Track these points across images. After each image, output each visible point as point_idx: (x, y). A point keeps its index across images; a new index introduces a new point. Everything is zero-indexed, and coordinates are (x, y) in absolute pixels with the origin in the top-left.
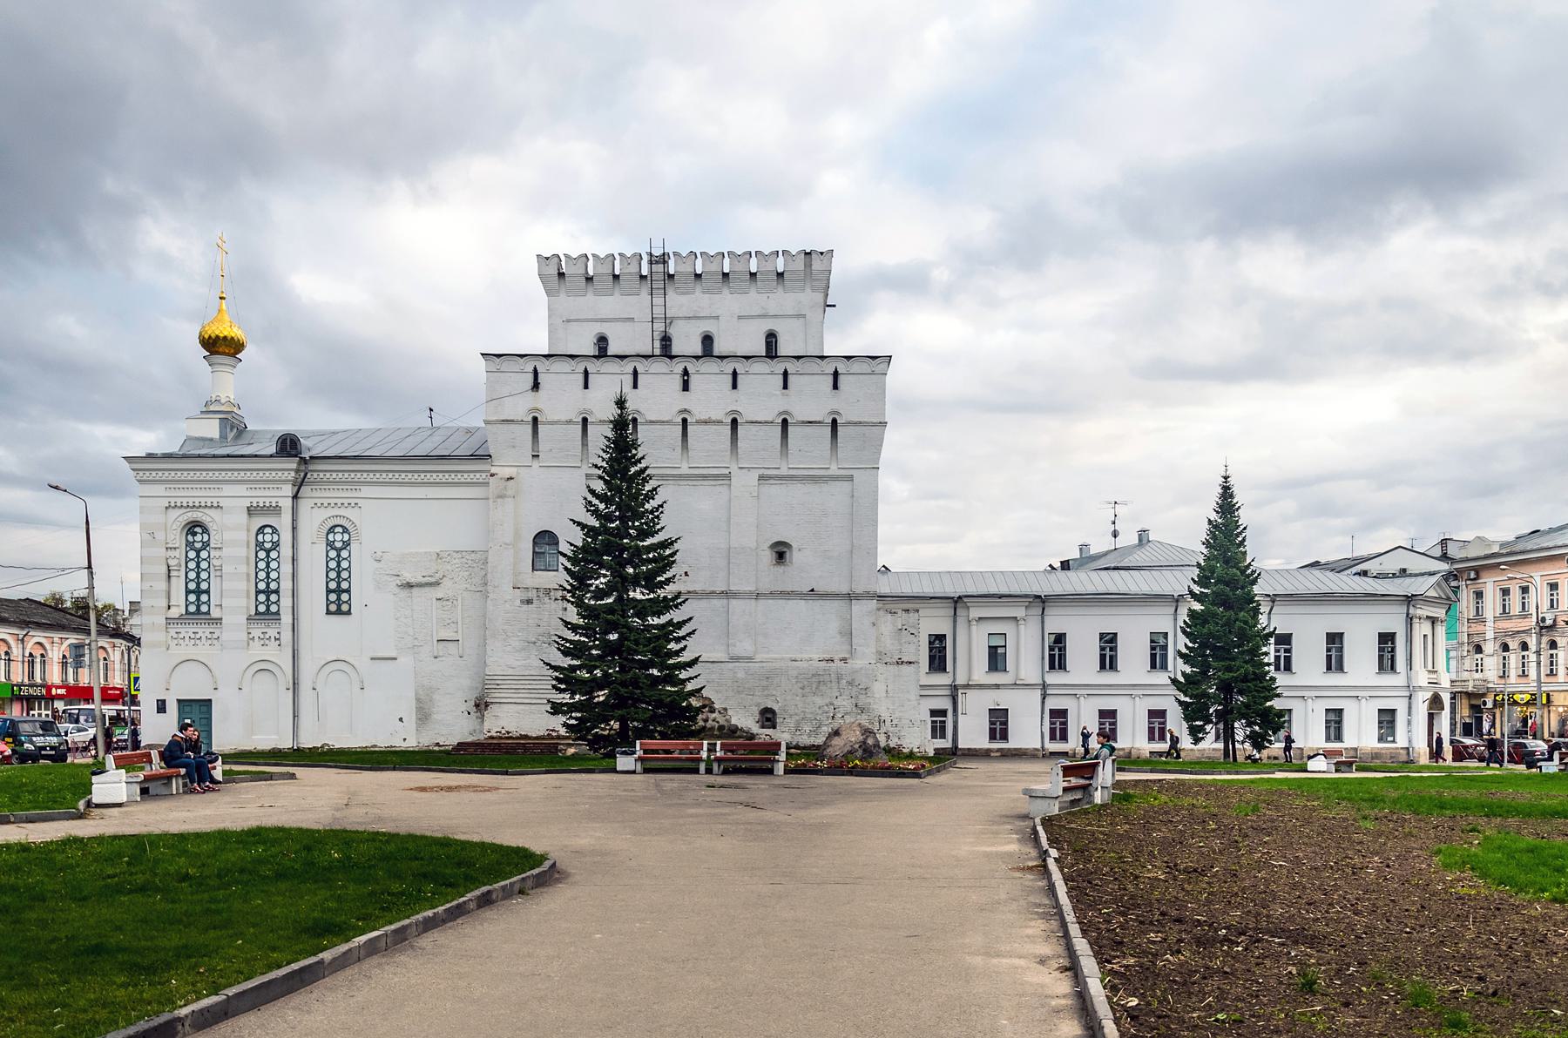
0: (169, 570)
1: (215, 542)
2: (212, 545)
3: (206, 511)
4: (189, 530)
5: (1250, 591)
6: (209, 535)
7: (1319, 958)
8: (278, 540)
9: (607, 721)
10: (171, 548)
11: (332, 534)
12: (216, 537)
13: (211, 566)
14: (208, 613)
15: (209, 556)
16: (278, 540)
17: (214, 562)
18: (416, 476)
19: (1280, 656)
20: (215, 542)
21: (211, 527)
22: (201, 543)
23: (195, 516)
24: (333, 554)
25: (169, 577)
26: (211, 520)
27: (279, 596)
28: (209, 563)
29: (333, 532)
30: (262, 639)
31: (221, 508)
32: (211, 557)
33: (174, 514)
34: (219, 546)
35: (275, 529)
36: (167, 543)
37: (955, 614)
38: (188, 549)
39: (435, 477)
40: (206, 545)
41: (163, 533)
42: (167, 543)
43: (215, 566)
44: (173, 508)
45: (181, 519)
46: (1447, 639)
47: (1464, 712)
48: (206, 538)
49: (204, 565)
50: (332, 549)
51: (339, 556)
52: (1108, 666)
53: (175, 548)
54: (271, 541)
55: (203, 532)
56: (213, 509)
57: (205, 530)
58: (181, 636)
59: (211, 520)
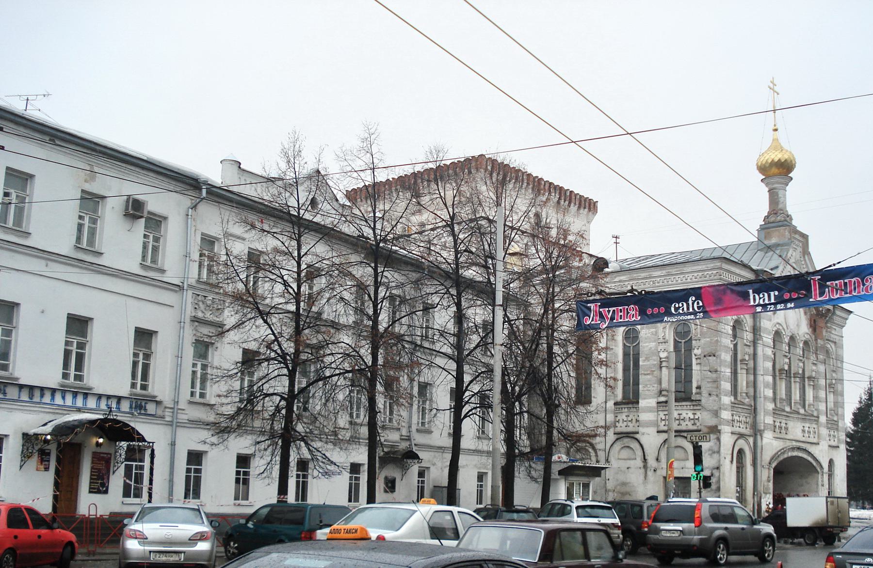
0: (661, 362)
43: (695, 355)
58: (630, 419)
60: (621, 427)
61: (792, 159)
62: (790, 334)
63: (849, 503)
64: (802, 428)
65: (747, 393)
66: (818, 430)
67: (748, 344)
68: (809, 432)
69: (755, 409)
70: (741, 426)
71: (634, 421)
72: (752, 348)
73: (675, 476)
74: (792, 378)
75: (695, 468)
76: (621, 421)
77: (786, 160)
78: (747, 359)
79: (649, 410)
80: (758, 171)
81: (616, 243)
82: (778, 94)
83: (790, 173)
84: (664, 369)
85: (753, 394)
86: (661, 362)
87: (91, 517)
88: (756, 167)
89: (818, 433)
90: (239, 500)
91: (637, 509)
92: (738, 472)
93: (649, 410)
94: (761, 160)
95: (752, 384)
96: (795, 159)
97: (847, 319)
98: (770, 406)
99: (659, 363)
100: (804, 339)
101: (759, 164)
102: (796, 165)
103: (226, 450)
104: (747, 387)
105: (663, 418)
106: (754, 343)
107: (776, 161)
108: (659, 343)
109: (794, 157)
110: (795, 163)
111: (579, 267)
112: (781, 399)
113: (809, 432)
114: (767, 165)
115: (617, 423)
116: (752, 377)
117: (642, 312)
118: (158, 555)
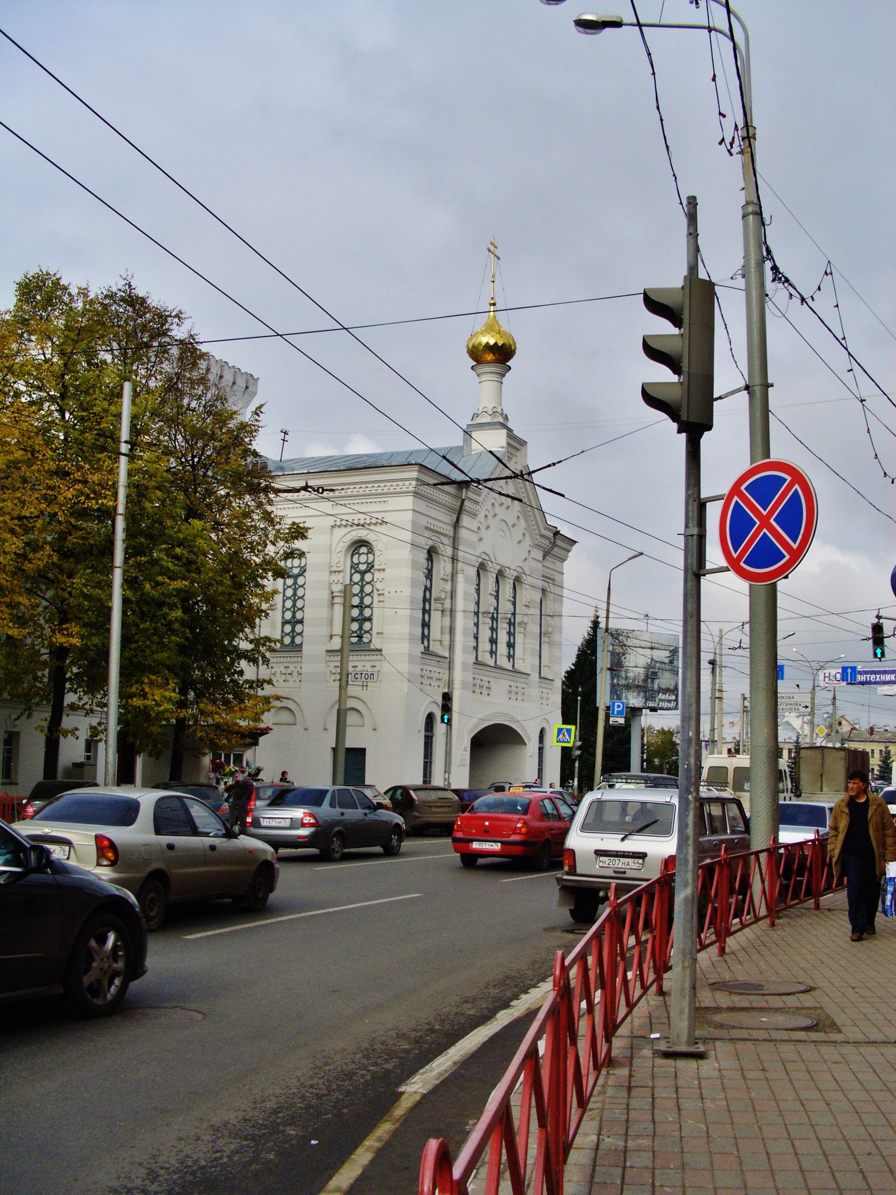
4: (354, 551)
6: (374, 555)
7: (322, 1099)
8: (373, 561)
9: (248, 693)
10: (335, 572)
12: (380, 558)
13: (375, 591)
16: (373, 561)
17: (378, 585)
22: (366, 565)
24: (357, 577)
27: (372, 624)
28: (373, 586)
29: (358, 553)
32: (375, 580)
33: (339, 533)
36: (331, 566)
37: (650, 1019)
38: (353, 571)
40: (370, 567)
41: (328, 555)
42: (331, 566)
43: (378, 590)
44: (339, 526)
45: (345, 539)
46: (4, 745)
47: (56, 436)
49: (368, 589)
50: (357, 572)
51: (362, 579)
53: (339, 572)
54: (366, 562)
55: (369, 553)
57: (371, 551)
58: (289, 671)
61: (512, 343)
63: (7, 794)
65: (441, 641)
67: (446, 577)
71: (295, 674)
72: (449, 583)
73: (347, 746)
74: (123, 460)
76: (278, 674)
80: (468, 355)
81: (284, 440)
82: (499, 259)
83: (508, 361)
86: (333, 598)
88: (466, 349)
90: (737, 769)
91: (724, 770)
94: (473, 341)
95: (448, 630)
96: (515, 344)
97: (569, 551)
101: (470, 345)
102: (517, 351)
103: (77, 733)
105: (334, 671)
108: (331, 572)
109: (514, 341)
110: (516, 348)
114: (481, 348)
116: (447, 620)
117: (104, 432)
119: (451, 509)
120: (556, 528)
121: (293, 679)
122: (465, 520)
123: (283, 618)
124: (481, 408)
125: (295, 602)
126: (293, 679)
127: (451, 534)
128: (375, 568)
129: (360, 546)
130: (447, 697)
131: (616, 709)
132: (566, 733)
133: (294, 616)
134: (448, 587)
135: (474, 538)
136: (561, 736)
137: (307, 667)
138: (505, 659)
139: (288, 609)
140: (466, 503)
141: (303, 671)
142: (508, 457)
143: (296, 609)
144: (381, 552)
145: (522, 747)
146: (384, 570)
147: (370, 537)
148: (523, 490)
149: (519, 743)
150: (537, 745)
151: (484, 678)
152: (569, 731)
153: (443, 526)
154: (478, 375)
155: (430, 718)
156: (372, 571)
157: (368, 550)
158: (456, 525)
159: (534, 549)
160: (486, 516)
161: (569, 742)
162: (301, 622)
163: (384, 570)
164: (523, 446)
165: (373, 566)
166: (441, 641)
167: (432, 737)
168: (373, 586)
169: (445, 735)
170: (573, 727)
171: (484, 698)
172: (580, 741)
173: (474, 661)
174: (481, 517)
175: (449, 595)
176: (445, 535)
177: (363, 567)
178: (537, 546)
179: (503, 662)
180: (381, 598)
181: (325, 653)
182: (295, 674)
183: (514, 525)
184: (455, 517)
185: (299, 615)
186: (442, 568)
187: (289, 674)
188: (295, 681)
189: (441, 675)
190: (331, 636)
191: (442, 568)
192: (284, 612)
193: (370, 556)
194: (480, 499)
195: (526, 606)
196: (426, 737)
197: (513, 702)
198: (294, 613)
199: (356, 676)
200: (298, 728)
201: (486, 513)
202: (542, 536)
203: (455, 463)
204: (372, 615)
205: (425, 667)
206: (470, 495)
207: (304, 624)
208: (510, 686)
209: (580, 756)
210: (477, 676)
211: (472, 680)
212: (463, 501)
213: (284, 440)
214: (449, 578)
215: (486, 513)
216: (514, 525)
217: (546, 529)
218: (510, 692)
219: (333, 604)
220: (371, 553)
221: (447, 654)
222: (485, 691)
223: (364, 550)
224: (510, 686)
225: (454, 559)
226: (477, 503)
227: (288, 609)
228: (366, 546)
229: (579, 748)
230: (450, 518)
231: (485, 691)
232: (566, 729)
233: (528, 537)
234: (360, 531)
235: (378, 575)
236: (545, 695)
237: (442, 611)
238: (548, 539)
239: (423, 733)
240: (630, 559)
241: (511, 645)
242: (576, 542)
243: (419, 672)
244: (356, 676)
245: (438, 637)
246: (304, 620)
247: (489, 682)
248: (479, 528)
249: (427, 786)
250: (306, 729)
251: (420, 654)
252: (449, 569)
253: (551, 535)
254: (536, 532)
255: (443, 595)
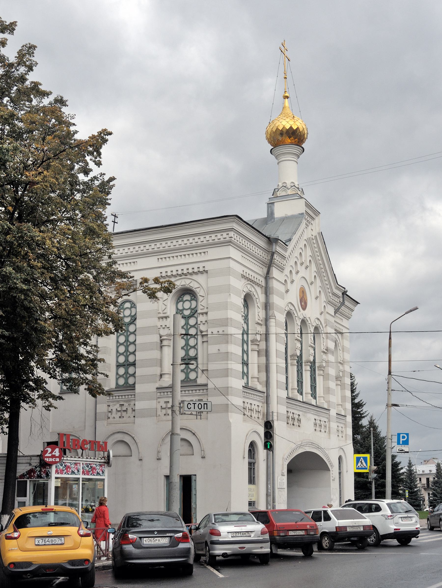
0: (161, 341)
1: (202, 308)
2: (199, 311)
3: (194, 277)
5: (81, 359)
8: (136, 314)
11: (181, 303)
13: (199, 333)
14: (195, 380)
15: (197, 323)
18: (131, 249)
19: (251, 468)
20: (202, 308)
21: (200, 292)
23: (183, 283)
25: (161, 347)
26: (198, 286)
30: (119, 411)
31: (207, 272)
32: (199, 323)
34: (205, 311)
35: (133, 303)
39: (142, 248)
40: (194, 312)
43: (201, 332)
48: (194, 303)
52: (389, 489)
56: (200, 275)
58: (124, 408)
59: (198, 286)
60: (114, 418)
62: (302, 317)
64: (314, 421)
65: (258, 378)
66: (329, 424)
67: (260, 322)
68: (320, 426)
69: (268, 397)
70: (257, 408)
71: (130, 411)
72: (264, 327)
75: (197, 377)
76: (114, 410)
77: (298, 128)
78: (259, 339)
79: (147, 396)
81: (114, 222)
84: (165, 349)
85: (265, 379)
87: (429, 528)
89: (329, 427)
92: (250, 469)
93: (147, 396)
98: (283, 394)
99: (159, 342)
100: (315, 324)
104: (259, 371)
106: (267, 320)
107: (288, 128)
111: (88, 273)
112: (292, 389)
113: (320, 426)
115: (110, 414)
116: (263, 360)
118: (237, 534)
119: (263, 263)
120: (344, 288)
121: (128, 415)
122: (275, 272)
123: (117, 361)
124: (281, 185)
125: (127, 347)
126: (128, 415)
127: (263, 284)
128: (198, 312)
129: (184, 294)
130: (268, 425)
131: (401, 440)
132: (363, 461)
133: (127, 360)
134: (262, 330)
135: (282, 288)
136: (359, 464)
137: (140, 405)
138: (310, 397)
139: (121, 344)
140: (275, 256)
141: (137, 408)
142: (306, 224)
143: (128, 353)
144: (203, 298)
145: (329, 472)
146: (206, 313)
147: (194, 285)
148: (318, 254)
149: (327, 470)
150: (338, 471)
151: (295, 412)
152: (365, 459)
153: (256, 276)
154: (276, 158)
155: (252, 445)
156: (196, 315)
157: (191, 297)
158: (267, 276)
159: (328, 305)
160: (291, 271)
161: (366, 469)
162: (134, 364)
163: (206, 313)
164: (317, 216)
165: (197, 311)
166: (258, 378)
167: (254, 463)
168: (197, 329)
169: (266, 461)
170: (368, 456)
171: (296, 429)
172: (375, 465)
173: (287, 396)
174: (287, 271)
175: (264, 336)
176: (258, 285)
177: (187, 313)
178: (330, 302)
179: (308, 398)
180: (205, 339)
181: (155, 390)
182: (130, 411)
183: (312, 283)
184: (265, 270)
185: (131, 359)
186: (257, 314)
187: (124, 411)
188: (129, 417)
189: (260, 408)
190: (161, 376)
191: (257, 314)
192: (117, 357)
193: (133, 310)
194: (287, 254)
195: (324, 352)
196: (250, 464)
197: (318, 433)
198: (127, 357)
199: (189, 405)
200: (134, 459)
201: (291, 269)
202: (334, 294)
203: (261, 231)
204: (197, 354)
205: (246, 400)
206: (279, 249)
207: (136, 366)
208: (315, 419)
209: (375, 479)
210: (289, 410)
211: (286, 413)
212: (273, 254)
213: (114, 222)
214: (263, 323)
215: (291, 269)
216: (312, 283)
217: (337, 288)
218: (315, 424)
219: (161, 347)
220: (193, 300)
221: (265, 390)
222: (296, 423)
223: (187, 297)
224: (315, 419)
225: (267, 306)
226: (284, 257)
227: (121, 344)
228: (189, 294)
229: (376, 472)
230: (262, 271)
231: (296, 423)
232: (363, 458)
233: (323, 294)
234: (183, 280)
235: (201, 318)
236: (340, 429)
237: (258, 352)
238: (339, 297)
239: (247, 460)
240: (407, 313)
241: (313, 387)
242: (358, 303)
243: (242, 404)
244: (189, 405)
245: (256, 375)
246: (137, 362)
247: (299, 415)
248: (286, 281)
249: (424, 473)
250: (141, 460)
251: (242, 388)
252: (262, 314)
253: (340, 294)
254: (329, 291)
255: (258, 337)
